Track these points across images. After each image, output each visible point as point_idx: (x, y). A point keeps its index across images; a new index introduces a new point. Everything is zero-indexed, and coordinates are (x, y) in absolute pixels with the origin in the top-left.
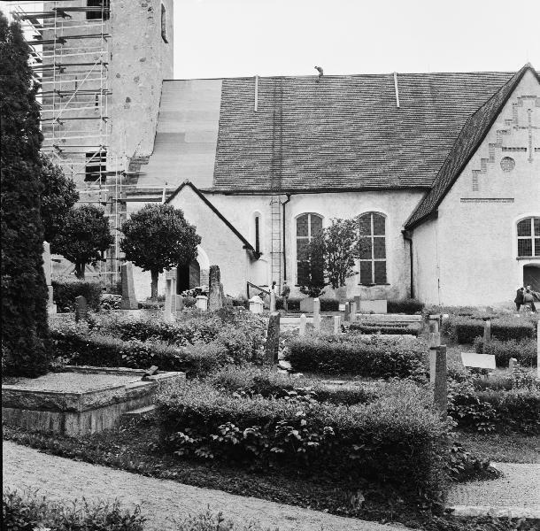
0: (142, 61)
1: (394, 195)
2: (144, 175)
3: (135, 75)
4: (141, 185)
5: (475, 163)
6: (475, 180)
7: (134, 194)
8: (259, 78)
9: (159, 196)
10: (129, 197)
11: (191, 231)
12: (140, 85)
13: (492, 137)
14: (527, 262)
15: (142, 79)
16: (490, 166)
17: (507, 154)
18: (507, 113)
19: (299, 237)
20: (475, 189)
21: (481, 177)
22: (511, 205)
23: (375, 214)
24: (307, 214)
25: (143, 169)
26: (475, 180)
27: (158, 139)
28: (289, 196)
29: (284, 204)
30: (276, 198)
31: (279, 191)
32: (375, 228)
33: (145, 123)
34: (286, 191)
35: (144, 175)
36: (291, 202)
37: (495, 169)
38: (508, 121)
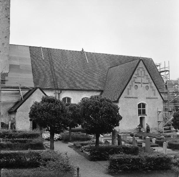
0: (6, 37)
1: (72, 91)
2: (7, 80)
3: (3, 42)
4: (7, 84)
5: (128, 87)
6: (128, 91)
7: (5, 88)
8: (42, 48)
9: (17, 89)
10: (2, 89)
11: (45, 101)
12: (5, 46)
13: (132, 79)
14: (140, 116)
15: (6, 44)
16: (132, 87)
17: (136, 84)
18: (136, 72)
19: (144, 109)
20: (128, 94)
21: (130, 91)
22: (136, 100)
23: (143, 103)
24: (66, 97)
25: (6, 78)
26: (128, 91)
27: (11, 67)
28: (61, 91)
29: (59, 94)
30: (57, 91)
31: (58, 89)
32: (142, 106)
33: (6, 61)
34: (60, 89)
35: (7, 80)
36: (61, 93)
37: (133, 88)
38: (136, 74)
